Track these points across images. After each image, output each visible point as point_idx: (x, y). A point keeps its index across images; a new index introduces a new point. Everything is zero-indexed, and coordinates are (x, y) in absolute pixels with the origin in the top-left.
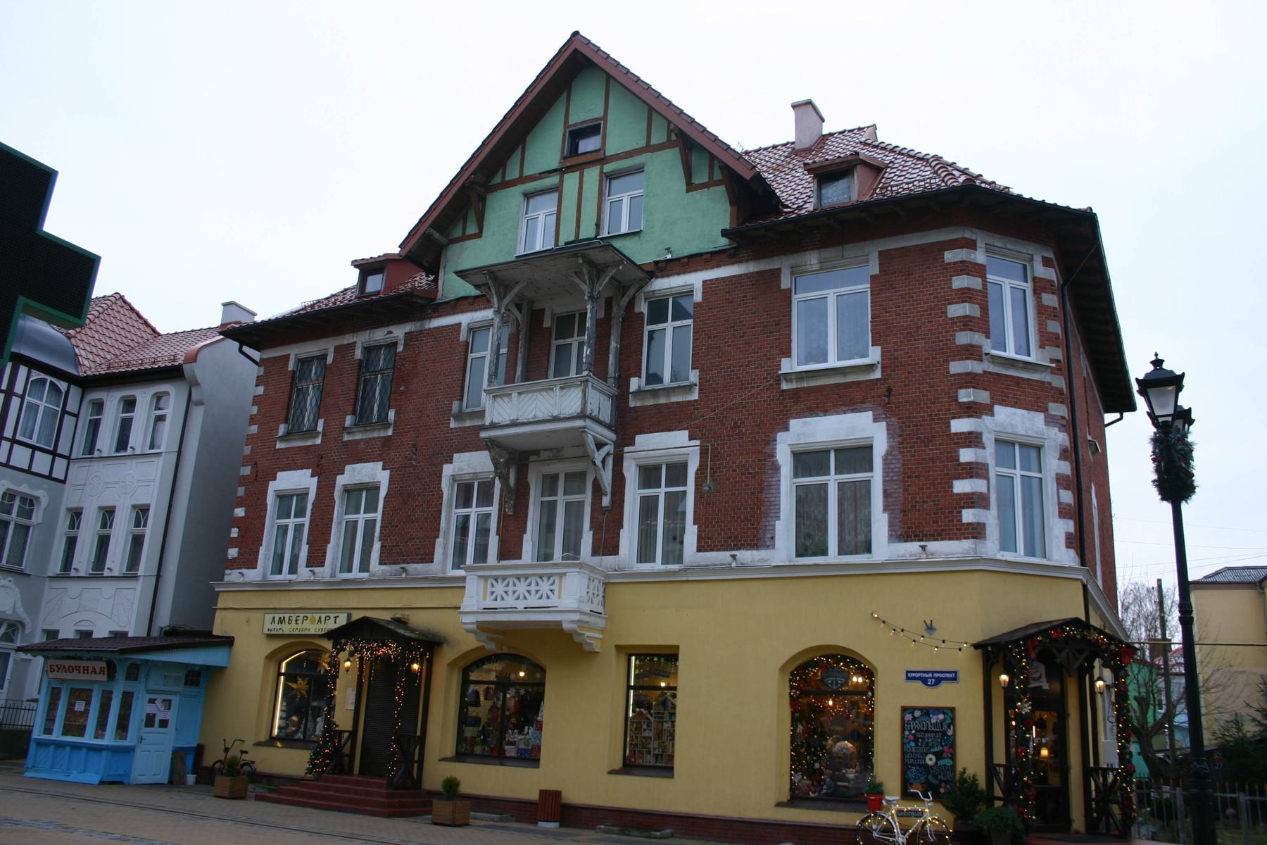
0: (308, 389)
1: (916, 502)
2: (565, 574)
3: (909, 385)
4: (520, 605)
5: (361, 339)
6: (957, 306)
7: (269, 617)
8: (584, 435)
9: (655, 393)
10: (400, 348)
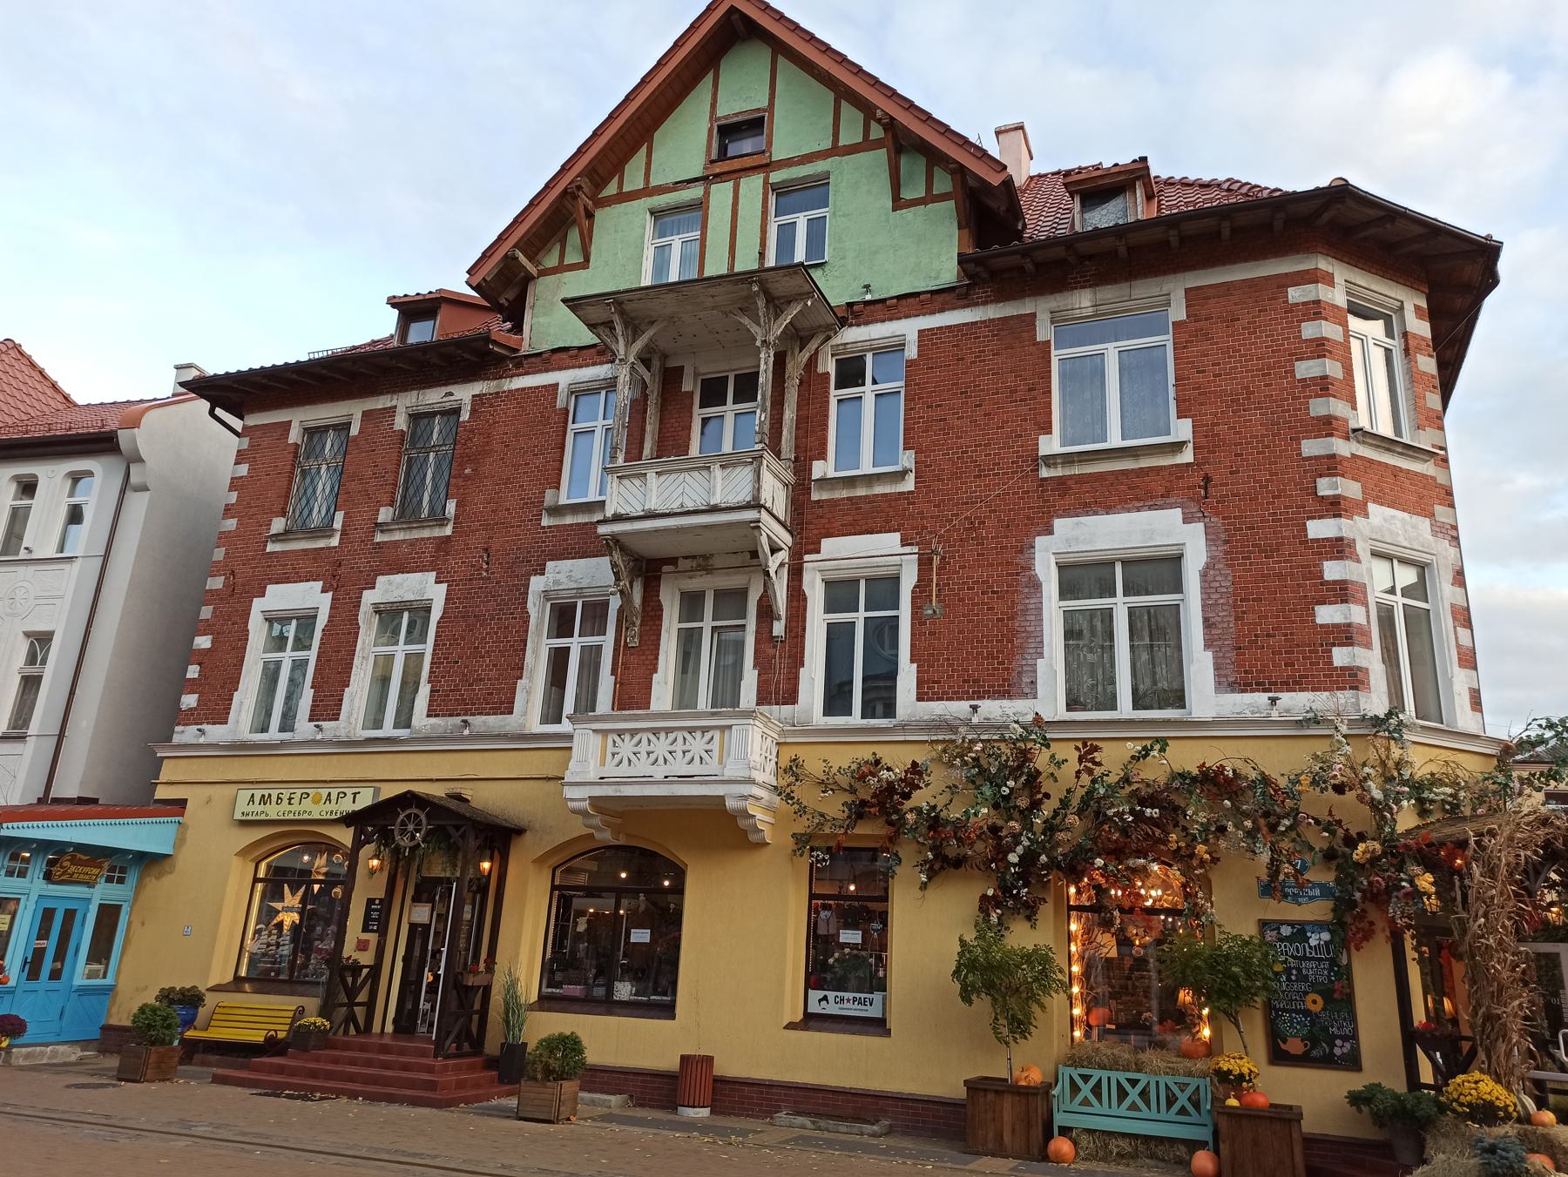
0: (319, 469)
1: (1256, 636)
2: (730, 727)
3: (1238, 472)
4: (659, 772)
5: (403, 405)
6: (1311, 363)
7: (244, 795)
8: (756, 532)
9: (850, 482)
10: (465, 416)
